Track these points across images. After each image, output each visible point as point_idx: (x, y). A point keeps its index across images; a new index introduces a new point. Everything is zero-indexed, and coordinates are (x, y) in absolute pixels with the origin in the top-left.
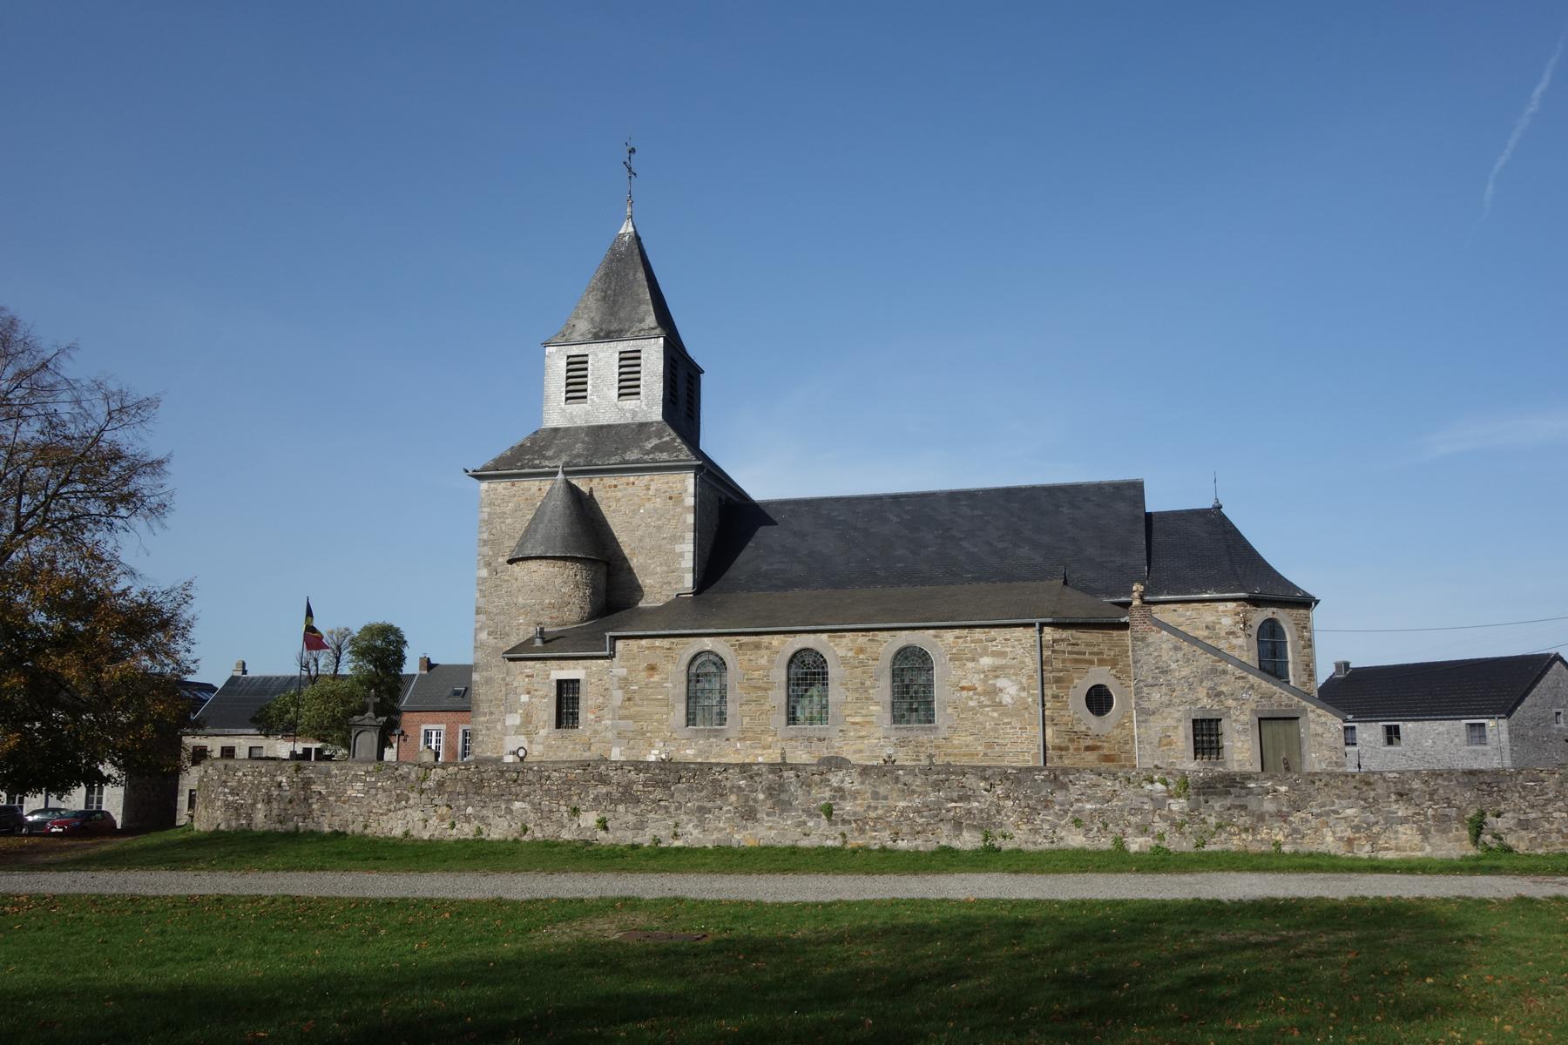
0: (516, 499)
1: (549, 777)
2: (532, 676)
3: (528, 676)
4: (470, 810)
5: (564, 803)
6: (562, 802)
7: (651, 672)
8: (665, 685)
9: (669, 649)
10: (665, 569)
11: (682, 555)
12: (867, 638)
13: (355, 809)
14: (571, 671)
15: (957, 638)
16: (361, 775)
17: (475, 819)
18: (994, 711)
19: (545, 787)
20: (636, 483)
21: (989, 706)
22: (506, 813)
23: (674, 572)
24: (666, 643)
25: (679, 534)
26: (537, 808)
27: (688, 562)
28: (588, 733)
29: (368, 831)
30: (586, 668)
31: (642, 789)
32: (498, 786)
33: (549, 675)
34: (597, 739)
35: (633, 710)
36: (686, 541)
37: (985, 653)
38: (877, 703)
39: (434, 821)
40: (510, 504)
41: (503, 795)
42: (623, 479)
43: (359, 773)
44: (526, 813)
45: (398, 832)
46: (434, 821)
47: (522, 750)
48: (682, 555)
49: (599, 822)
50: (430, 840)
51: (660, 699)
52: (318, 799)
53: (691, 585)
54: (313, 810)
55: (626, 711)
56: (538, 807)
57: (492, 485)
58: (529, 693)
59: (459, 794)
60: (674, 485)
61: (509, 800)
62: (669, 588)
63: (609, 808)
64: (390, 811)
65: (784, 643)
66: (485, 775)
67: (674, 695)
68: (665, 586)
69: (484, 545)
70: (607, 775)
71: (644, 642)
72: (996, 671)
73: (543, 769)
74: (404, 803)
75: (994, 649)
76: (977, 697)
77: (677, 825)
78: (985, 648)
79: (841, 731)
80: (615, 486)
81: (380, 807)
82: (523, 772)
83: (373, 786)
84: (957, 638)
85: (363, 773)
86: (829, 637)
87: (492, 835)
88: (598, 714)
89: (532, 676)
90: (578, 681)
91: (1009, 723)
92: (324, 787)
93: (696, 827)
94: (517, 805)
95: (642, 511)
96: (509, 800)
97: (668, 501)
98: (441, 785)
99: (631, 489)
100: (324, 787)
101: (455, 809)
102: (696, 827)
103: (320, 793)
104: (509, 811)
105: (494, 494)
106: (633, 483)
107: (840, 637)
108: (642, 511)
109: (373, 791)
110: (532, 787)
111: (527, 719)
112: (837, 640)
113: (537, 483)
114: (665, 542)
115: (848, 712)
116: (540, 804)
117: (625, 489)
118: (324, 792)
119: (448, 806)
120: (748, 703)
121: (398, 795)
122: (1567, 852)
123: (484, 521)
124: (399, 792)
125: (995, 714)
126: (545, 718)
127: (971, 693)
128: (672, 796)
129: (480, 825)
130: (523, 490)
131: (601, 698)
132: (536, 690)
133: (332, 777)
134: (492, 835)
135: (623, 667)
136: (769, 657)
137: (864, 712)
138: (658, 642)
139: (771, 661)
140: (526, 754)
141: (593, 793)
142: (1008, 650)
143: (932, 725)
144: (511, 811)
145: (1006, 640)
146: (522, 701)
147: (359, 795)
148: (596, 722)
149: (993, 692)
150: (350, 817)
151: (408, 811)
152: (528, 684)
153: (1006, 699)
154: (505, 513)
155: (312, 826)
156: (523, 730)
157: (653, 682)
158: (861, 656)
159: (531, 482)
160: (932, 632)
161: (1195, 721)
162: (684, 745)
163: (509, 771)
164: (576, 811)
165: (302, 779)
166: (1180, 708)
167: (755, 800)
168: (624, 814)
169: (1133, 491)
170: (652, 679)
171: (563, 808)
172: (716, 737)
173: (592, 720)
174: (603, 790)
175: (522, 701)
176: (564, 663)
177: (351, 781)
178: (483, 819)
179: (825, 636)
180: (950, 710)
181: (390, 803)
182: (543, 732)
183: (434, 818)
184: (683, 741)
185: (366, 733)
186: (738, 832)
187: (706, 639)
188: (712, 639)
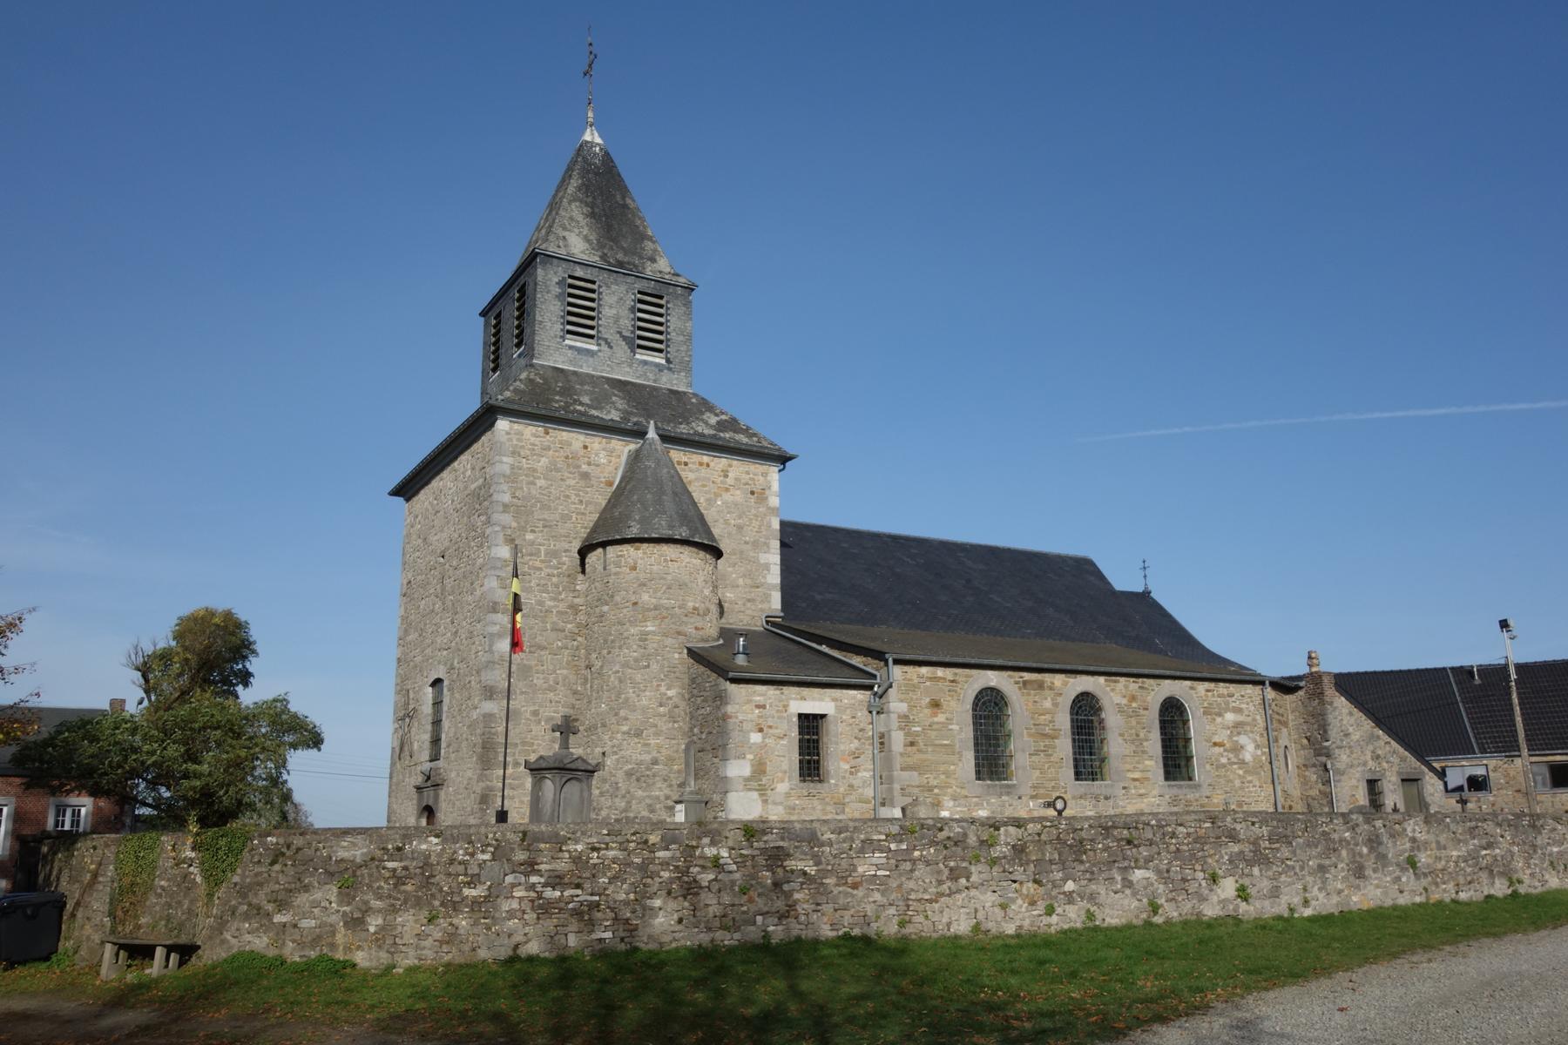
0: (551, 452)
1: (1174, 835)
2: (763, 707)
3: (758, 707)
4: (1070, 886)
5: (1200, 868)
6: (1198, 867)
7: (936, 710)
8: (950, 727)
9: (953, 681)
10: (749, 581)
11: (767, 567)
12: (1137, 685)
13: (877, 896)
14: (817, 703)
15: (1208, 691)
16: (880, 840)
17: (1082, 898)
18: (1240, 768)
19: (1173, 848)
20: (712, 464)
21: (1235, 763)
22: (1123, 886)
23: (758, 587)
24: (947, 673)
25: (763, 540)
26: (1164, 875)
27: (774, 577)
28: (842, 790)
29: (909, 930)
30: (834, 700)
31: (1268, 846)
32: (1106, 848)
33: (788, 705)
34: (853, 797)
35: (916, 758)
36: (773, 551)
37: (1227, 710)
38: (1151, 758)
39: (1019, 906)
40: (543, 459)
41: (1114, 862)
42: (695, 456)
43: (875, 837)
44: (1152, 884)
45: (962, 927)
46: (1019, 906)
47: (1059, 800)
48: (767, 567)
49: (1238, 890)
50: (1018, 936)
51: (946, 745)
52: (802, 884)
53: (780, 607)
54: (796, 902)
55: (908, 759)
56: (1166, 875)
57: (516, 426)
58: (761, 730)
59: (1051, 862)
60: (756, 478)
61: (1125, 869)
62: (753, 607)
63: (1246, 871)
64: (943, 895)
65: (1065, 684)
66: (1083, 834)
67: (961, 741)
68: (749, 605)
69: (504, 512)
70: (1235, 829)
71: (924, 670)
72: (1238, 727)
73: (1164, 823)
74: (963, 881)
75: (1234, 704)
76: (1226, 754)
77: (1305, 889)
78: (1227, 703)
79: (1124, 788)
80: (686, 464)
81: (925, 891)
82: (1136, 828)
83: (906, 856)
84: (1208, 691)
85: (883, 837)
86: (1106, 680)
87: (1108, 920)
88: (853, 762)
89: (763, 707)
90: (823, 716)
91: (1250, 782)
92: (811, 863)
93: (1320, 889)
94: (1138, 875)
95: (719, 503)
96: (1125, 869)
97: (749, 495)
98: (1019, 850)
99: (704, 471)
100: (811, 863)
101: (1050, 886)
102: (1320, 889)
103: (805, 873)
104: (1128, 884)
105: (518, 440)
106: (708, 465)
107: (1115, 682)
108: (719, 503)
109: (908, 866)
110: (1154, 848)
111: (759, 769)
112: (1112, 684)
113: (582, 438)
114: (745, 547)
115: (1128, 767)
116: (1168, 871)
117: (698, 470)
118: (811, 870)
119: (1035, 881)
120: (1036, 753)
121: (951, 870)
122: (1567, 887)
123: (504, 476)
124: (952, 864)
125: (1241, 772)
126: (785, 766)
127: (1222, 749)
128: (1294, 852)
129: (1089, 906)
130: (560, 442)
131: (856, 741)
132: (770, 727)
133: (822, 845)
134: (1108, 920)
135: (902, 701)
136: (1052, 700)
137: (1140, 766)
138: (940, 672)
139: (1055, 705)
140: (1065, 808)
141: (1226, 853)
142: (1243, 706)
143: (1191, 783)
144: (1131, 882)
145: (1242, 696)
146: (752, 741)
147: (879, 873)
148: (851, 773)
149: (1237, 749)
150: (870, 909)
151: (973, 892)
152: (759, 717)
153: (1248, 757)
154: (535, 470)
155: (796, 930)
156: (754, 784)
157: (938, 723)
158: (1134, 705)
159: (573, 435)
160: (1188, 683)
161: (1368, 781)
162: (977, 804)
163: (1116, 828)
164: (1214, 879)
165: (763, 851)
166: (1359, 769)
167: (1361, 855)
168: (1260, 880)
169: (1084, 569)
170: (936, 719)
171: (1200, 875)
172: (1008, 794)
173: (846, 771)
174: (1236, 848)
175: (752, 741)
176: (806, 691)
177: (862, 851)
178: (1092, 898)
179: (1102, 679)
180: (1208, 767)
181: (940, 883)
182: (782, 787)
183: (1020, 901)
184: (975, 800)
185: (573, 782)
186: (1355, 894)
187: (990, 673)
188: (996, 673)
